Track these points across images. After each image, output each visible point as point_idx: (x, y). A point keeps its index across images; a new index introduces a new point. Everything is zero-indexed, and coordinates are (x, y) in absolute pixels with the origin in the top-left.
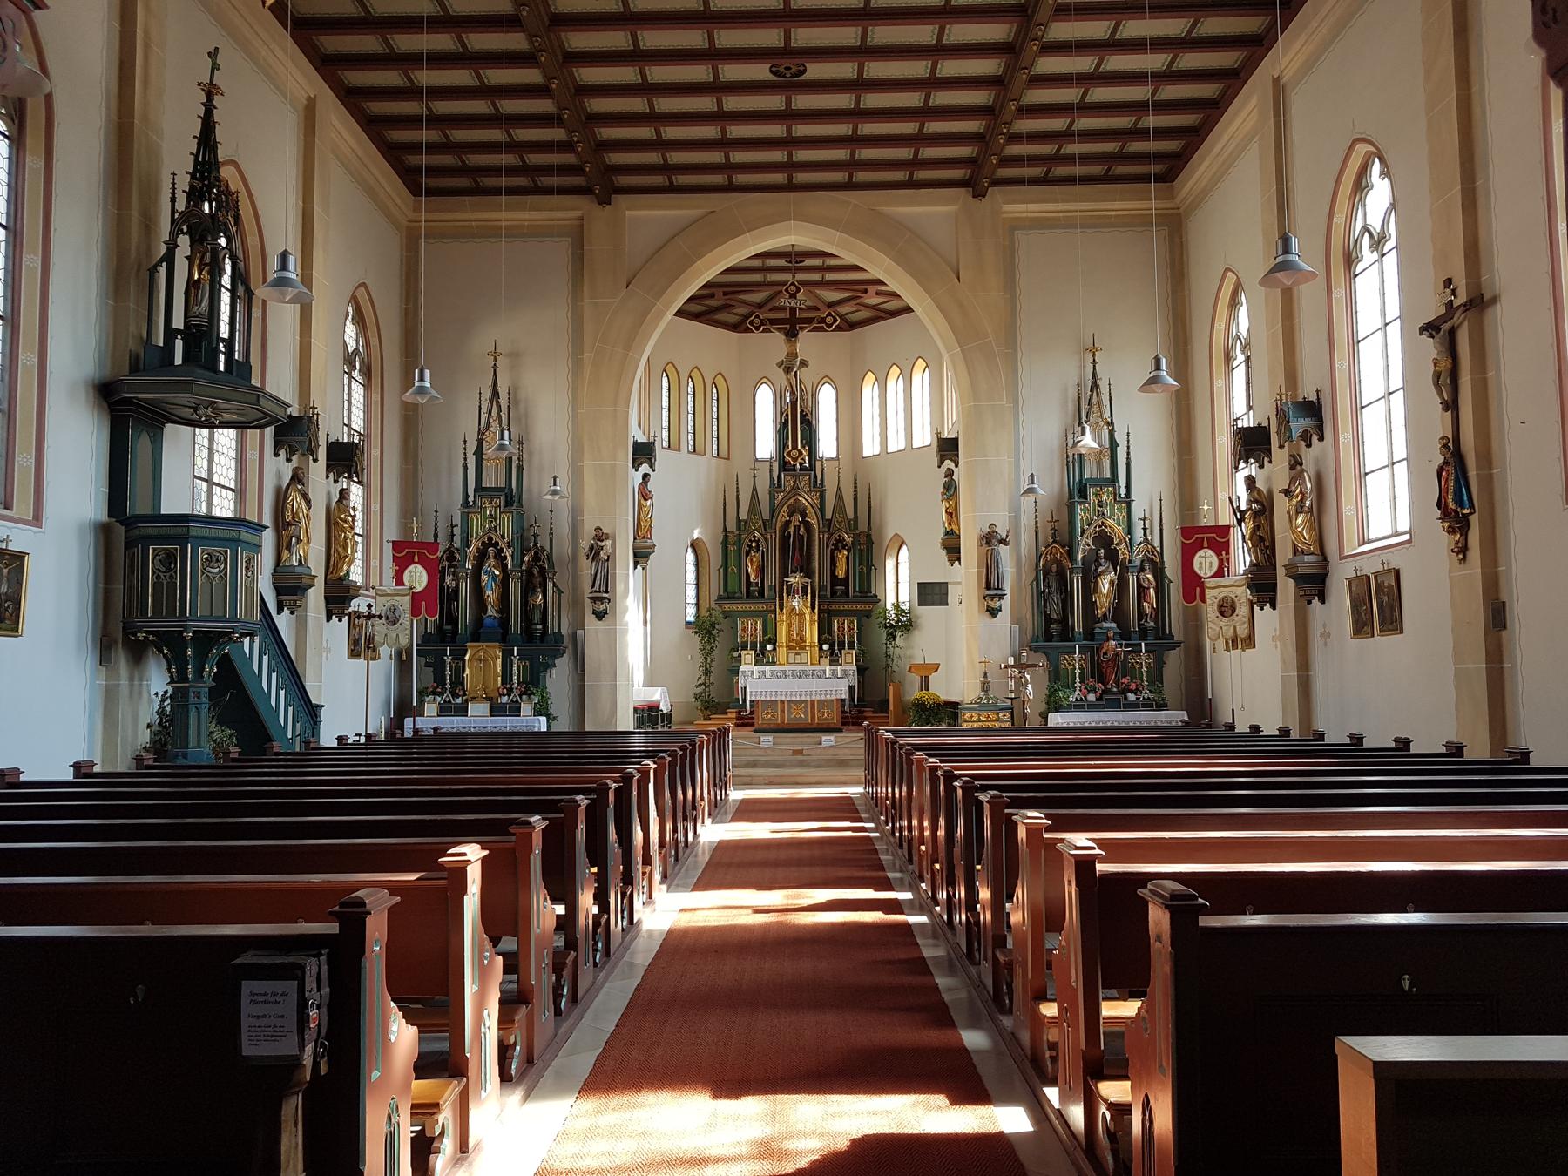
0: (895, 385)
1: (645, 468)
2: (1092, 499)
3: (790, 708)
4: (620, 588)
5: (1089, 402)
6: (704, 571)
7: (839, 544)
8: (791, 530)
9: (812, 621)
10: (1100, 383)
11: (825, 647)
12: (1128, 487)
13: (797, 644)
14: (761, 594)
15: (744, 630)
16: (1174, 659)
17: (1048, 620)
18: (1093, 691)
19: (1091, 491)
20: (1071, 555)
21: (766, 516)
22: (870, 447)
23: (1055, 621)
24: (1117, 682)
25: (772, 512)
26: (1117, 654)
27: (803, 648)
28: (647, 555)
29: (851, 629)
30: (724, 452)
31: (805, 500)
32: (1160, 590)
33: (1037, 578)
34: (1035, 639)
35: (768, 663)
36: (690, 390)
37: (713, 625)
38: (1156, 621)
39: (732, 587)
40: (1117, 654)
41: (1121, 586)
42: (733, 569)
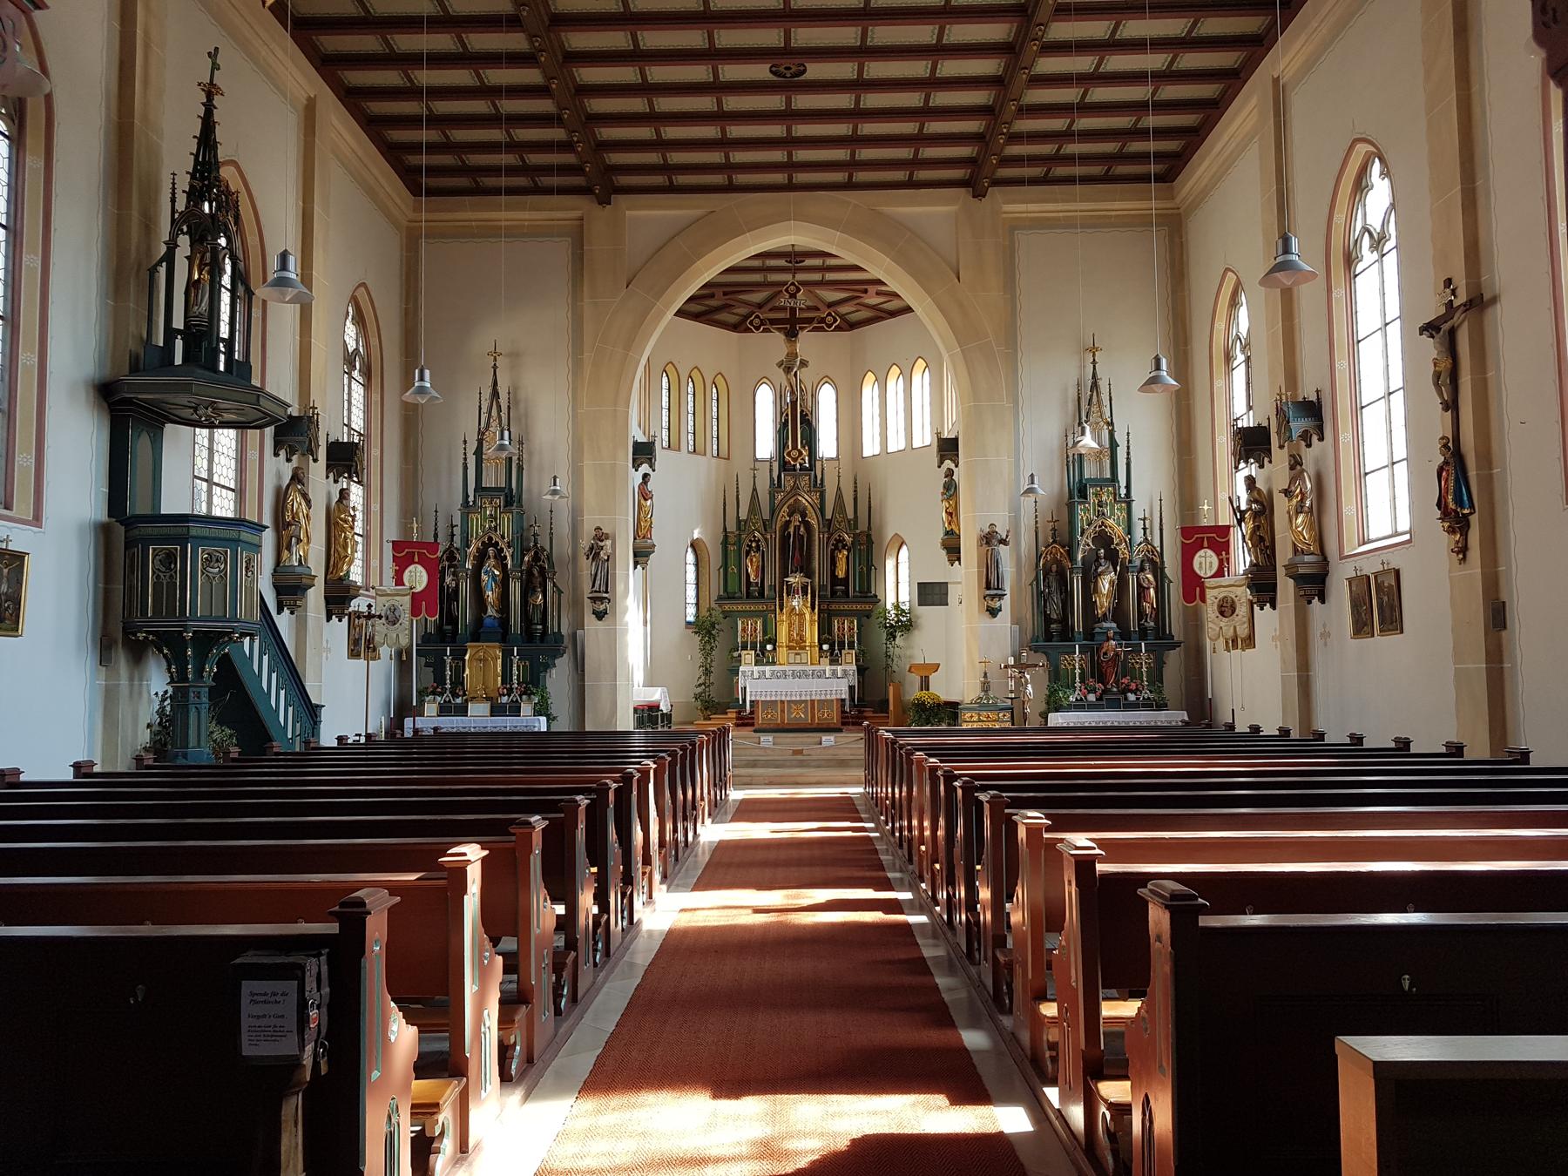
0: (895, 385)
1: (645, 468)
2: (1092, 499)
3: (790, 708)
4: (620, 588)
5: (1089, 402)
6: (704, 571)
7: (839, 544)
8: (791, 530)
9: (812, 621)
10: (1100, 383)
11: (825, 647)
12: (1128, 487)
13: (797, 644)
14: (761, 594)
15: (744, 630)
16: (1174, 659)
17: (1048, 620)
18: (1093, 691)
19: (1091, 491)
20: (1071, 555)
21: (766, 516)
22: (870, 447)
23: (1055, 621)
24: (1117, 682)
25: (772, 512)
26: (1117, 654)
27: (803, 648)
28: (647, 555)
29: (851, 629)
30: (724, 452)
31: (805, 500)
32: (1160, 590)
33: (1037, 578)
34: (1035, 639)
35: (768, 663)
36: (690, 390)
37: (713, 625)
38: (1156, 621)
39: (732, 587)
40: (1117, 654)
41: (1121, 586)
42: (733, 569)
